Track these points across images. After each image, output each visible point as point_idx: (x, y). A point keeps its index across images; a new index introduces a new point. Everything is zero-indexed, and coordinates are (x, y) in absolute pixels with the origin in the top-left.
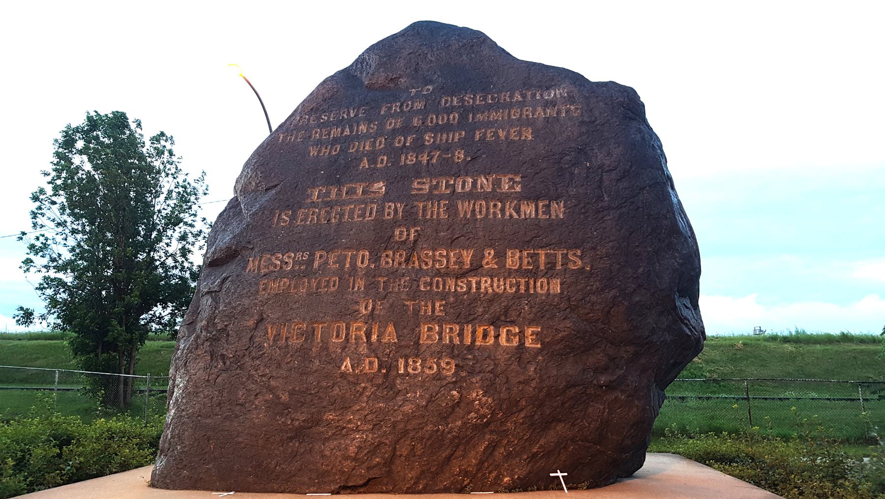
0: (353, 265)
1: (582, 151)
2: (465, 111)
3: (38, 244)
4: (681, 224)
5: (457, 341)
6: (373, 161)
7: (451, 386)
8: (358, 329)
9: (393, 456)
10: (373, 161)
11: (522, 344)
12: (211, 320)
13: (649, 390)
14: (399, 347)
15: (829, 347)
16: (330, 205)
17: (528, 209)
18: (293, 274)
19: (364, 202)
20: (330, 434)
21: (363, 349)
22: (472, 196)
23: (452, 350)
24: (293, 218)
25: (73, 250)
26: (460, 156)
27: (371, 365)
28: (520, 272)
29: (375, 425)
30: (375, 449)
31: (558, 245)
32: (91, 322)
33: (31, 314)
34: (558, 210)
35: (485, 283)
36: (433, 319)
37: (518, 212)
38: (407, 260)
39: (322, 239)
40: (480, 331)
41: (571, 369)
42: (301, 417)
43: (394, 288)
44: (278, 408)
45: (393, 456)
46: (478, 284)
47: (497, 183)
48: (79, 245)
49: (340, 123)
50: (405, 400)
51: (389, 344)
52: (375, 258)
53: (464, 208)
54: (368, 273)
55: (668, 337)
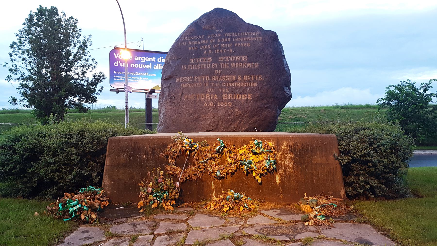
0: (205, 80)
1: (262, 50)
2: (232, 38)
3: (13, 68)
4: (286, 68)
5: (232, 98)
6: (207, 51)
8: (208, 96)
9: (218, 124)
10: (207, 51)
11: (247, 98)
12: (169, 94)
13: (276, 110)
14: (218, 100)
15: (360, 110)
16: (197, 64)
17: (249, 65)
18: (189, 82)
19: (206, 63)
21: (209, 100)
22: (235, 62)
24: (187, 67)
25: (29, 70)
26: (231, 50)
27: (211, 104)
28: (247, 81)
30: (214, 123)
31: (256, 74)
32: (44, 103)
33: (16, 100)
34: (256, 65)
35: (239, 84)
36: (226, 93)
37: (247, 66)
38: (219, 79)
39: (196, 73)
40: (237, 95)
41: (259, 104)
42: (196, 116)
43: (216, 85)
44: (189, 114)
45: (218, 124)
46: (237, 84)
47: (241, 58)
48: (33, 69)
49: (197, 40)
50: (220, 112)
51: (216, 99)
52: (210, 78)
53: (233, 65)
54: (209, 82)
55: (281, 96)
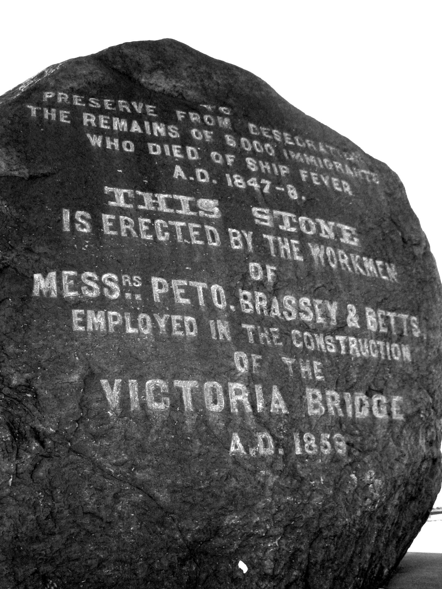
7: (349, 468)
20: (236, 546)
23: (341, 424)
29: (285, 527)
53: (316, 251)
